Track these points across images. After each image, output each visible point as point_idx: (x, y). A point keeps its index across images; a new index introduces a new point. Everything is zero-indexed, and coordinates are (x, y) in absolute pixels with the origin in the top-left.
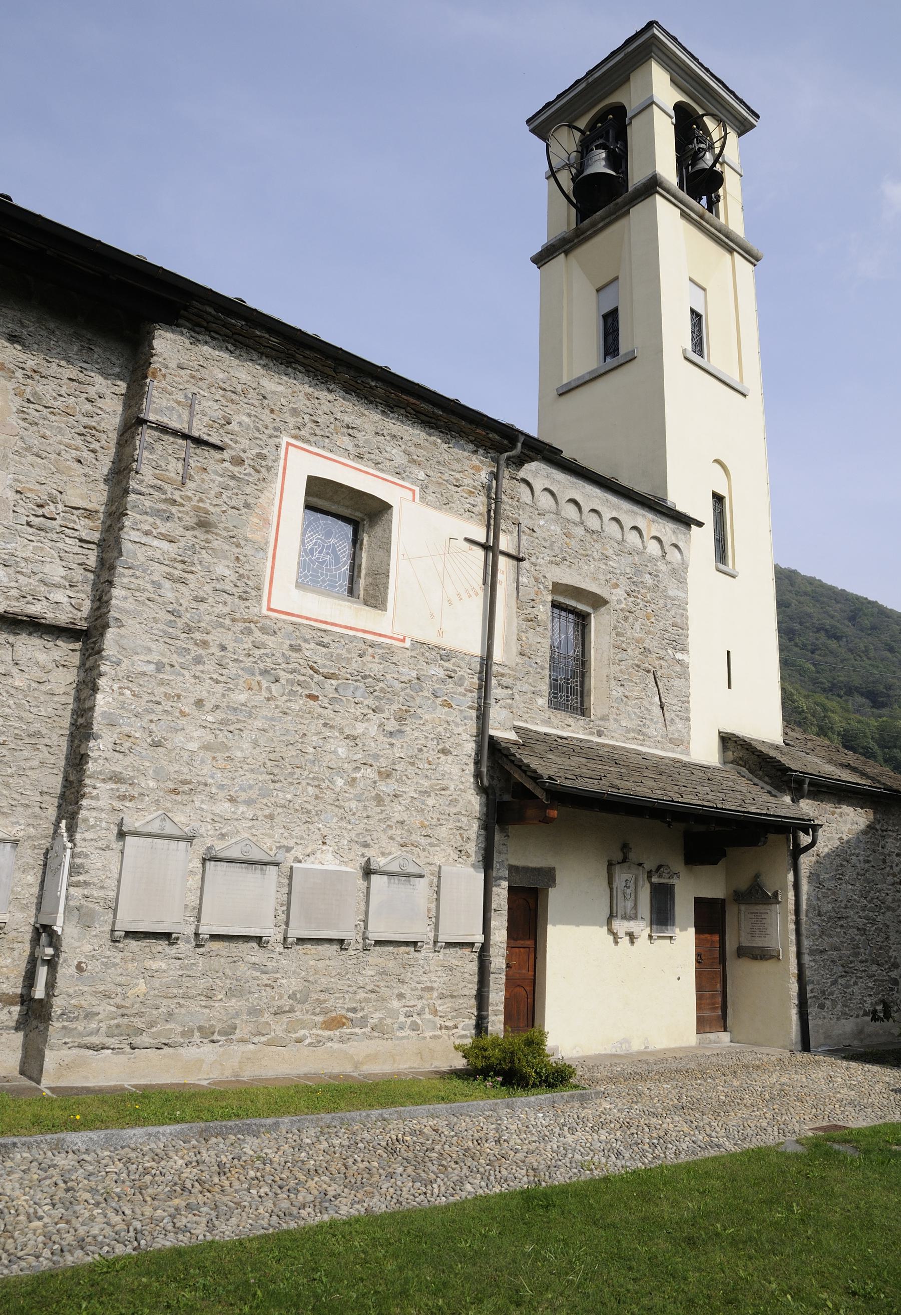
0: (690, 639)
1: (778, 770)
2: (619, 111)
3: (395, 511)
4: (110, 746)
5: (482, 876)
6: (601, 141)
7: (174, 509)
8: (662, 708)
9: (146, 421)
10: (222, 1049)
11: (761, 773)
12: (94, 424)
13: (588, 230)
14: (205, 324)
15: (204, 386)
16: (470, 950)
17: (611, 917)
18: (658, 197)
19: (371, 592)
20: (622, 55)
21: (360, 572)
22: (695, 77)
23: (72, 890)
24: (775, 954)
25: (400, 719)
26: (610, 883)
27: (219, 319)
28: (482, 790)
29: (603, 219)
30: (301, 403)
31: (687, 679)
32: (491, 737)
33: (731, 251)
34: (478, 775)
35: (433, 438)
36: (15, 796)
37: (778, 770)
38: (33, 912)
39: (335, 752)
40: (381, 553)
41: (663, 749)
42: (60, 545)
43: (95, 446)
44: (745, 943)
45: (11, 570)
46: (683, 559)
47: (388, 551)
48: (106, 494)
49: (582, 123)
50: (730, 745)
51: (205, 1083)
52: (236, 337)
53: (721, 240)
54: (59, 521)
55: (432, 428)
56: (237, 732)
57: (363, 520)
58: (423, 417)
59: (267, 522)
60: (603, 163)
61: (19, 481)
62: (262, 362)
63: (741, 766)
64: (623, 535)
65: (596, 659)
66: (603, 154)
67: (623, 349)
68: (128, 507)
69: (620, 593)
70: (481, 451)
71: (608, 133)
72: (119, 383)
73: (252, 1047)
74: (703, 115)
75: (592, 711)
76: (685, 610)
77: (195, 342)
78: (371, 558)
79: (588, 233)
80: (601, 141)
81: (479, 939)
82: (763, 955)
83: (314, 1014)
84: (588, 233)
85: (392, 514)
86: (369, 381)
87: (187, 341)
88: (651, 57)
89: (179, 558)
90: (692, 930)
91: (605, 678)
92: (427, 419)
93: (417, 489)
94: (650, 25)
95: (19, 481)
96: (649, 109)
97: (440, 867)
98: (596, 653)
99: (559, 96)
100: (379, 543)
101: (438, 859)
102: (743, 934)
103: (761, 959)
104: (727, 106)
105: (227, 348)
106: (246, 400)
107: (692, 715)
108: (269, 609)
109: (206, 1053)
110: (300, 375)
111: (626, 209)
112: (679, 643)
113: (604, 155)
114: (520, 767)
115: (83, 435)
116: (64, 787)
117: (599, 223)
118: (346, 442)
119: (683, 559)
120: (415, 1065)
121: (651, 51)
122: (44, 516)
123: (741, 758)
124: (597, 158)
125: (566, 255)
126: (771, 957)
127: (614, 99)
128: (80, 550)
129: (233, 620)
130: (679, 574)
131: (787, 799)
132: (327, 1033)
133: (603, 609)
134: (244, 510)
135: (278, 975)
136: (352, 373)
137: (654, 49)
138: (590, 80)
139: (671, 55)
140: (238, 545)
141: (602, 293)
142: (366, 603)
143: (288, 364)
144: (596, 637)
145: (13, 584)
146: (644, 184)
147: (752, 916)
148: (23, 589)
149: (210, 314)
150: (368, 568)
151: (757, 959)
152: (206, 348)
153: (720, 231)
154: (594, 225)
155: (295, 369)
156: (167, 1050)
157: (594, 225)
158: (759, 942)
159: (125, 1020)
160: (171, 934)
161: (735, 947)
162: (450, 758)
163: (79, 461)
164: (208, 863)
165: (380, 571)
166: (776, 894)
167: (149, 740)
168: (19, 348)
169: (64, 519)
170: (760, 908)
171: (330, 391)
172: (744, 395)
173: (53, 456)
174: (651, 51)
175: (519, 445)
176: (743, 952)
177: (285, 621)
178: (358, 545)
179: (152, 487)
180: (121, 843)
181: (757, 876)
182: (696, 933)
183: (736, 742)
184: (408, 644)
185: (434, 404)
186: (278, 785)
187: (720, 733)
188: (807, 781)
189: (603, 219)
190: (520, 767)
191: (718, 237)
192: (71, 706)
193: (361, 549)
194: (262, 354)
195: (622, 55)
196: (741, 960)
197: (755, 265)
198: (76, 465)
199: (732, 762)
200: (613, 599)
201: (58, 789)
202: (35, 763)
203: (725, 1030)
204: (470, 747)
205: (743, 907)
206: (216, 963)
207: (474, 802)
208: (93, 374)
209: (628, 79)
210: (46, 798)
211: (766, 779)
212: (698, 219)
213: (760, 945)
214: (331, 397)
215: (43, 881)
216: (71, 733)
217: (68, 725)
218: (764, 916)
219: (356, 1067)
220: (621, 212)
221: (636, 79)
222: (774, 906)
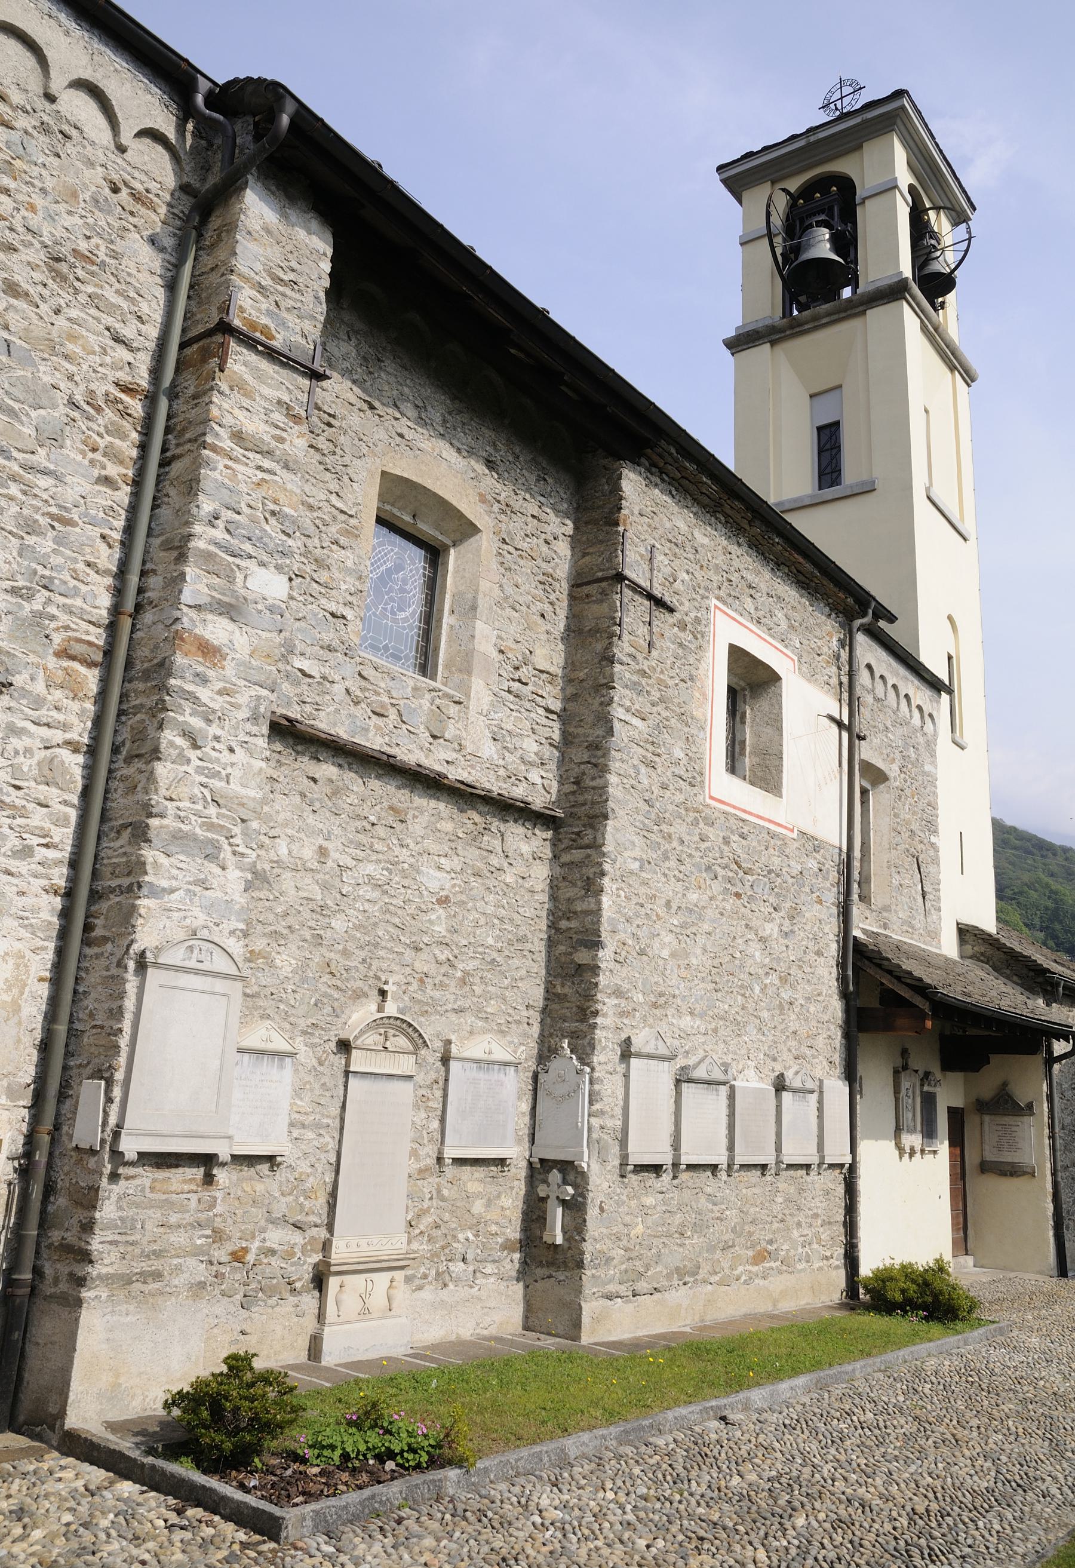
0: (939, 820)
1: (1033, 970)
2: (847, 186)
3: (784, 681)
4: (612, 955)
5: (847, 1089)
6: (823, 217)
7: (644, 681)
8: (924, 898)
9: (625, 578)
10: (692, 1291)
11: (1008, 972)
12: (550, 570)
13: (807, 323)
14: (661, 464)
15: (657, 536)
16: (838, 1171)
17: (898, 1130)
18: (905, 303)
19: (759, 774)
20: (857, 120)
21: (743, 749)
22: (928, 159)
23: (593, 1120)
24: (1029, 1170)
25: (792, 918)
26: (897, 1092)
27: (676, 461)
28: (845, 995)
29: (828, 314)
30: (720, 560)
31: (938, 865)
32: (855, 938)
33: (952, 368)
34: (843, 980)
35: (804, 600)
36: (511, 1011)
37: (1033, 970)
38: (527, 1145)
39: (753, 956)
40: (769, 730)
41: (924, 943)
42: (533, 715)
43: (553, 597)
44: (990, 1157)
45: (499, 745)
46: (935, 730)
47: (780, 730)
48: (562, 654)
49: (794, 185)
50: (968, 937)
51: (688, 1329)
52: (685, 482)
53: (947, 356)
54: (530, 688)
55: (803, 588)
56: (692, 936)
57: (744, 689)
58: (801, 578)
59: (704, 695)
60: (828, 246)
61: (502, 639)
62: (694, 510)
63: (982, 961)
64: (898, 704)
65: (875, 843)
66: (825, 234)
67: (851, 472)
68: (615, 679)
69: (895, 767)
70: (833, 616)
71: (831, 209)
72: (568, 522)
73: (709, 1287)
74: (930, 209)
75: (873, 900)
76: (935, 787)
77: (650, 484)
78: (757, 735)
79: (806, 327)
80: (823, 217)
81: (848, 1159)
82: (1013, 1171)
83: (747, 1248)
84: (806, 327)
85: (781, 688)
86: (774, 537)
87: (644, 483)
88: (893, 130)
89: (651, 739)
90: (947, 1143)
91: (885, 865)
92: (804, 579)
93: (796, 658)
94: (899, 94)
95: (502, 639)
96: (889, 194)
97: (821, 1081)
98: (875, 835)
99: (766, 149)
100: (766, 719)
101: (818, 1073)
102: (986, 1147)
103: (1012, 1175)
104: (950, 195)
105: (670, 492)
106: (685, 555)
107: (942, 905)
108: (711, 798)
109: (678, 1296)
110: (720, 526)
111: (861, 308)
112: (931, 826)
113: (827, 236)
114: (890, 972)
115: (544, 583)
116: (546, 999)
117: (823, 317)
118: (749, 604)
119: (935, 730)
120: (810, 1301)
121: (895, 124)
122: (520, 681)
123: (982, 954)
124: (821, 238)
125: (772, 346)
126: (1024, 1173)
127: (843, 166)
128: (545, 721)
129: (687, 810)
130: (931, 744)
131: (1040, 1002)
132: (755, 1269)
133: (882, 786)
134: (689, 683)
135: (723, 1207)
136: (764, 528)
137: (899, 122)
138: (812, 139)
139: (912, 131)
140: (687, 725)
141: (815, 399)
142: (752, 783)
143: (713, 513)
144: (875, 817)
145: (501, 762)
146: (890, 286)
147: (1000, 1128)
148: (509, 767)
149: (671, 454)
150: (753, 746)
151: (1006, 1175)
152: (657, 491)
153: (948, 347)
154: (815, 318)
155: (717, 518)
156: (657, 1295)
157: (815, 318)
158: (1008, 1157)
159: (630, 1264)
160: (661, 1166)
161: (977, 1161)
162: (822, 959)
163: (543, 616)
164: (684, 1086)
165: (770, 751)
166: (1030, 1106)
167: (637, 948)
168: (496, 476)
169: (535, 684)
170: (1007, 1120)
171: (739, 545)
172: (965, 539)
173: (524, 608)
174: (895, 124)
175: (870, 611)
176: (985, 1167)
177: (719, 810)
178: (738, 719)
179: (629, 655)
180: (624, 1066)
181: (1005, 1084)
182: (950, 1146)
183: (976, 935)
184: (795, 835)
185: (815, 564)
186: (719, 995)
187: (958, 924)
188: (1062, 983)
189: (828, 314)
190: (890, 972)
191: (945, 353)
192: (546, 906)
193: (743, 722)
194: (695, 500)
195: (857, 120)
196: (984, 1176)
197: (969, 385)
198: (540, 620)
199: (971, 957)
200: (891, 775)
201: (540, 1004)
202: (523, 972)
203: (967, 1254)
204: (833, 949)
205: (987, 1118)
206: (687, 1194)
207: (836, 1008)
208: (548, 511)
209: (859, 147)
210: (531, 1012)
211: (1015, 978)
212: (932, 330)
213: (1010, 1160)
214: (739, 552)
215: (534, 1108)
216: (549, 937)
217: (545, 928)
218: (1014, 1129)
219: (774, 1305)
220: (853, 311)
221: (871, 150)
222: (1026, 1118)
